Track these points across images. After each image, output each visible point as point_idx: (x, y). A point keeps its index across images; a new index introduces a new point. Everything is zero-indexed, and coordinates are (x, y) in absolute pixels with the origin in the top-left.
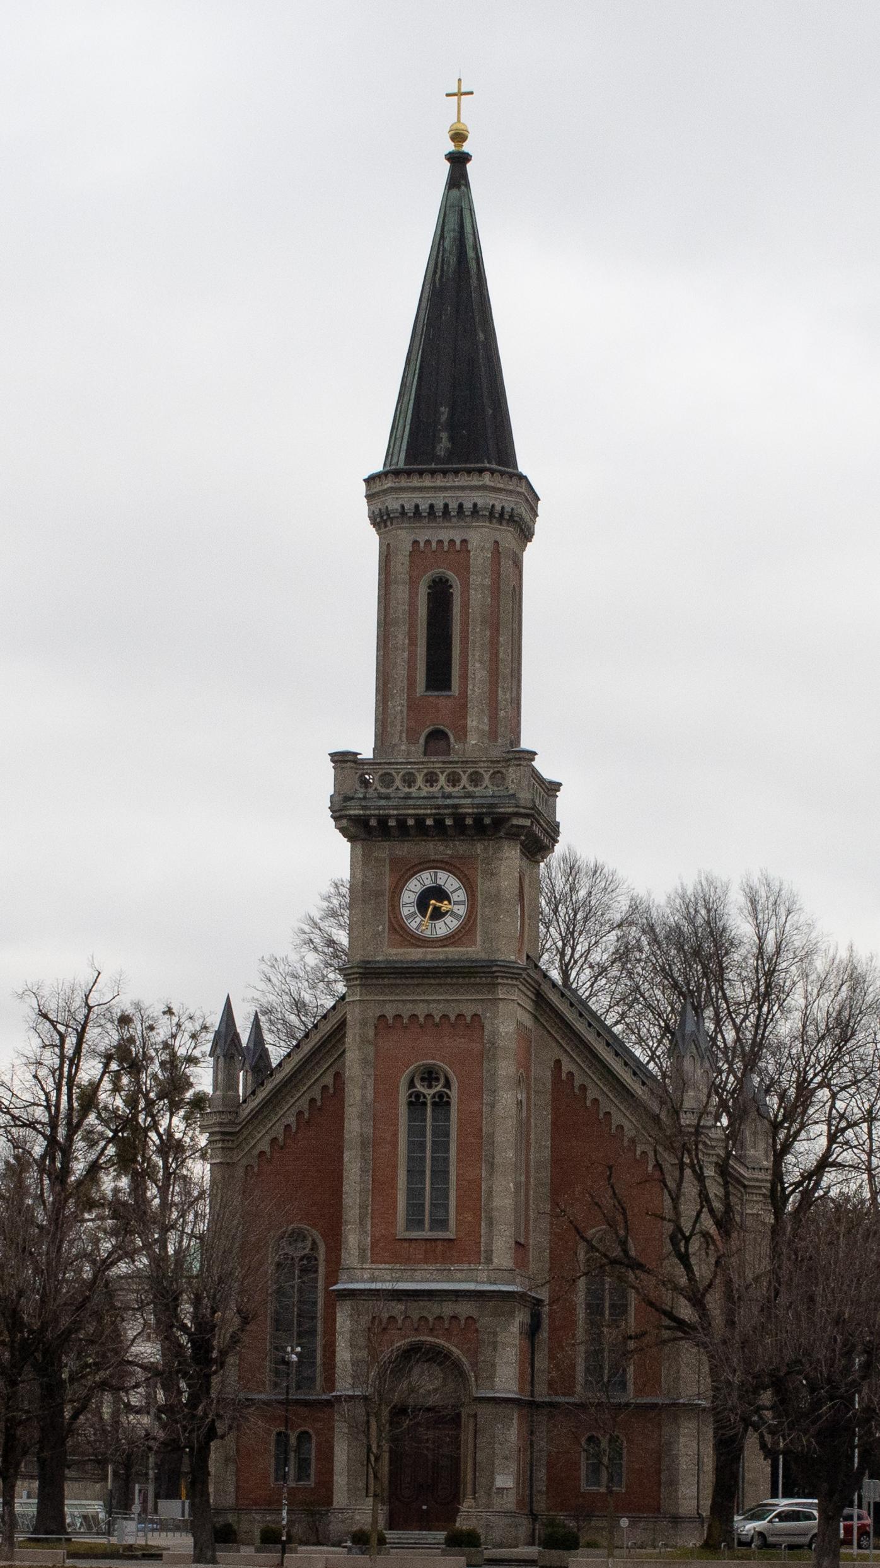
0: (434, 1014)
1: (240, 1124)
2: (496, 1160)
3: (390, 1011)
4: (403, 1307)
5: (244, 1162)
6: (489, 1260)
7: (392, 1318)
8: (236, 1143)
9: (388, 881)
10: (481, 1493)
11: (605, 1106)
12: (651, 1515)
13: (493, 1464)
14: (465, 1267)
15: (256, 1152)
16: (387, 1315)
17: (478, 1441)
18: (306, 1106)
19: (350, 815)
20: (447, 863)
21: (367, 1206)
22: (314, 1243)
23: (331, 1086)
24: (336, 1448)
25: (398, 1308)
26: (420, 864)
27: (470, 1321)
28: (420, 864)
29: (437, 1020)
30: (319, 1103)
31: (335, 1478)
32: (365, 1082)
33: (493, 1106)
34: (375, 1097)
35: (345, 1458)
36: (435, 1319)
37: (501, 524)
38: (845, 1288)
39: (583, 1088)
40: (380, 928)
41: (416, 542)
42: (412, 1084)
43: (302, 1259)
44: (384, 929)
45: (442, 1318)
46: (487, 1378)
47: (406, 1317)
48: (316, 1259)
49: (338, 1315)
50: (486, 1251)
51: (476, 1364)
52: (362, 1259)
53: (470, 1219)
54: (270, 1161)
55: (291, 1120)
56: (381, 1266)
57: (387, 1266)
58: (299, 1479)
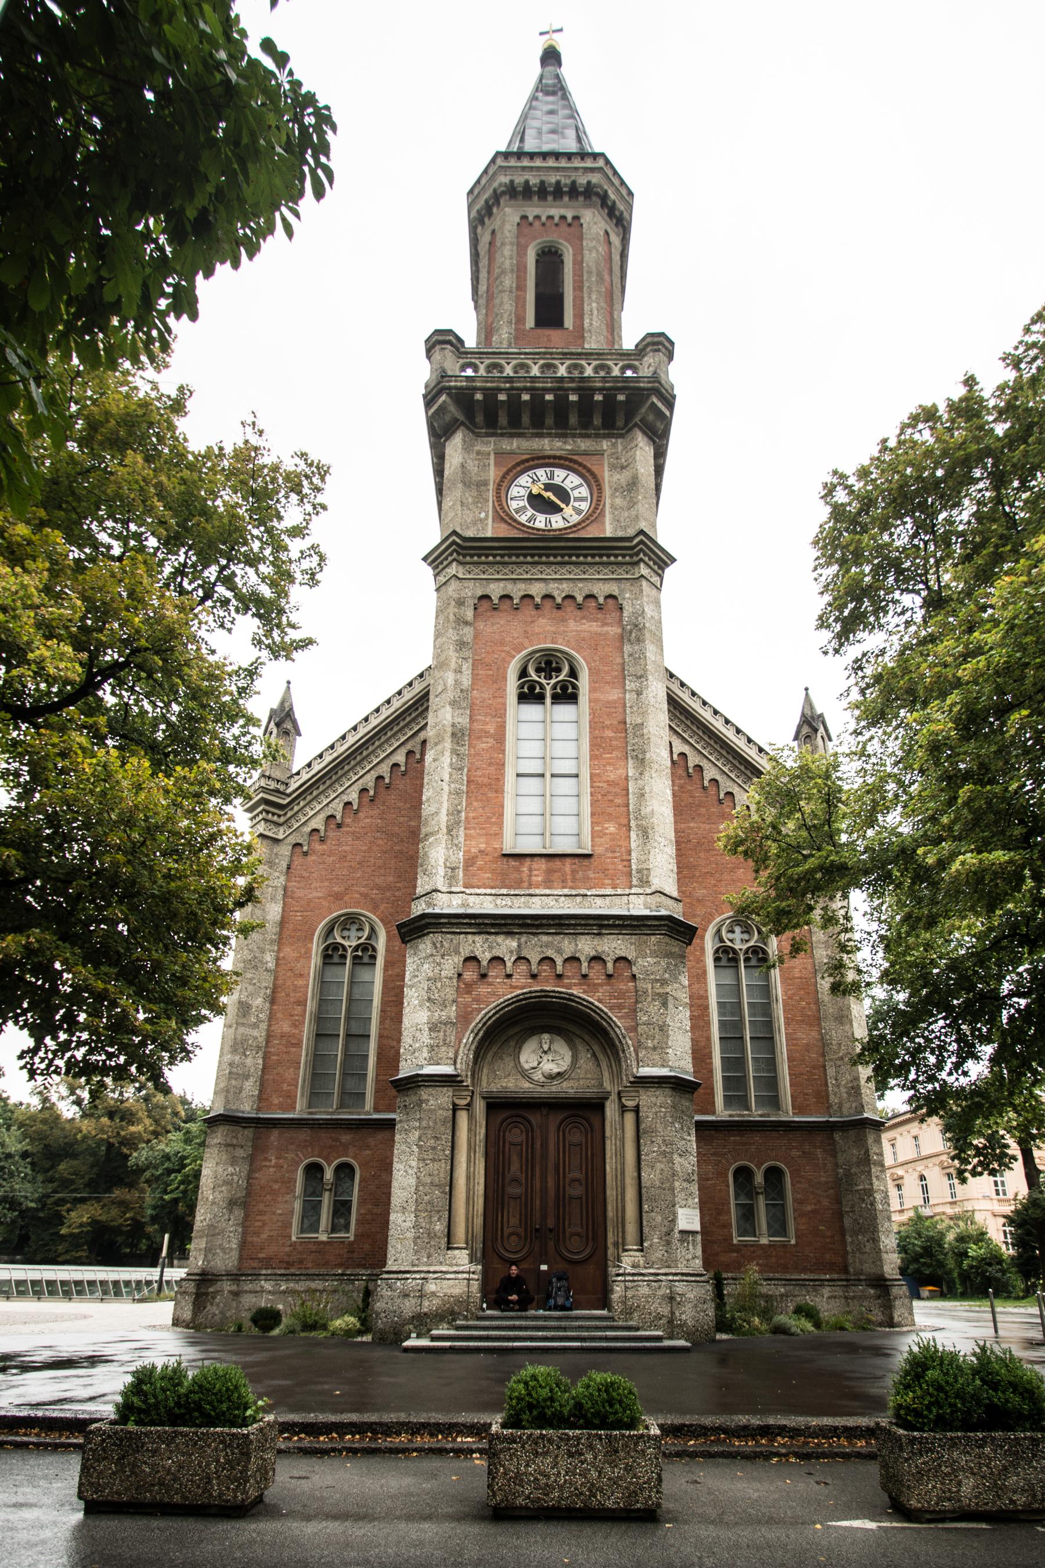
0: (555, 594)
1: (289, 795)
2: (648, 756)
3: (495, 590)
5: (292, 840)
6: (645, 882)
7: (497, 960)
8: (282, 820)
9: (492, 474)
10: (654, 1239)
11: (726, 785)
12: (835, 1276)
15: (307, 829)
16: (488, 956)
17: (645, 1150)
18: (371, 784)
19: (450, 388)
20: (566, 459)
21: (459, 812)
22: (373, 930)
23: (402, 764)
24: (396, 1166)
25: (506, 946)
26: (533, 459)
27: (622, 965)
28: (533, 459)
29: (559, 600)
30: (387, 781)
31: (393, 1217)
32: (461, 666)
33: (639, 693)
34: (473, 684)
35: (413, 1181)
37: (614, 202)
39: (699, 768)
40: (483, 515)
41: (524, 217)
42: (523, 673)
43: (356, 949)
44: (487, 515)
45: (578, 959)
46: (654, 1048)
48: (374, 949)
49: (408, 961)
51: (634, 1029)
52: (451, 879)
54: (322, 840)
55: (353, 796)
58: (334, 1230)
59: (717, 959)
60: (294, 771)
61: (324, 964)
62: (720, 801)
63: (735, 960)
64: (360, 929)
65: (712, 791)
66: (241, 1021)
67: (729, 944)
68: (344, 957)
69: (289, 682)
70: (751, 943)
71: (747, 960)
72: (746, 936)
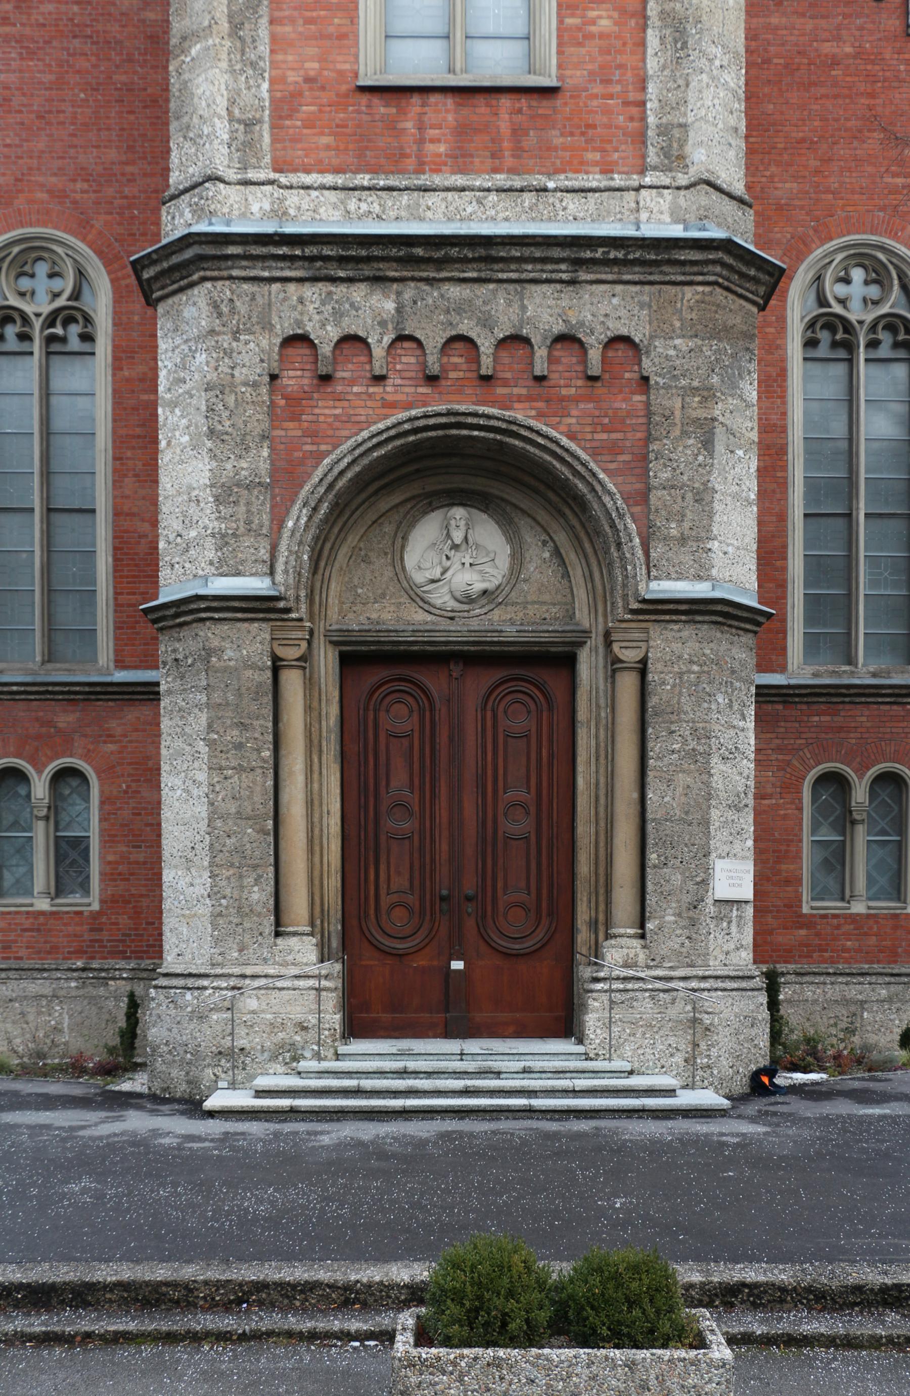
4: (390, 306)
13: (705, 823)
14: (594, 180)
16: (333, 333)
22: (81, 274)
24: (167, 780)
27: (621, 352)
35: (202, 810)
36: (502, 343)
38: (887, 736)
45: (526, 341)
47: (401, 338)
50: (664, 130)
51: (643, 497)
53: (604, 22)
56: (308, 179)
57: (329, 179)
59: (810, 343)
63: (849, 346)
67: (837, 309)
70: (885, 309)
72: (874, 291)
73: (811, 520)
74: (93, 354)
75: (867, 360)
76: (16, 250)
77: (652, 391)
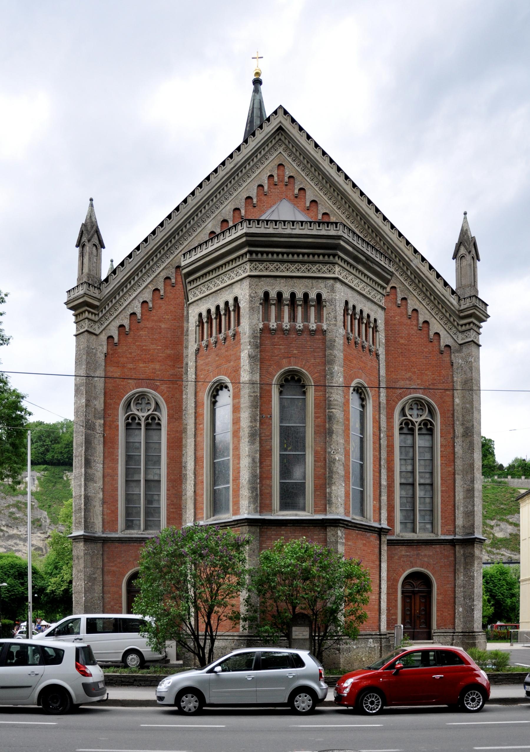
22: (157, 404)
59: (401, 429)
60: (103, 277)
61: (127, 429)
62: (441, 353)
63: (412, 430)
64: (148, 403)
65: (435, 342)
66: (401, 432)
67: (409, 417)
68: (139, 424)
69: (91, 200)
70: (423, 418)
71: (420, 429)
72: (420, 413)
73: (403, 486)
74: (161, 429)
75: (419, 434)
76: (137, 395)
77: (319, 205)
